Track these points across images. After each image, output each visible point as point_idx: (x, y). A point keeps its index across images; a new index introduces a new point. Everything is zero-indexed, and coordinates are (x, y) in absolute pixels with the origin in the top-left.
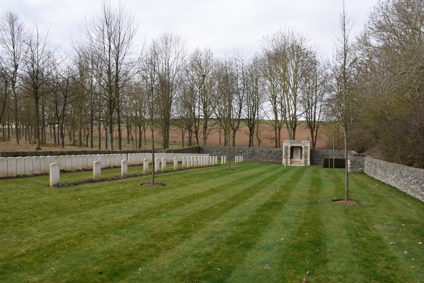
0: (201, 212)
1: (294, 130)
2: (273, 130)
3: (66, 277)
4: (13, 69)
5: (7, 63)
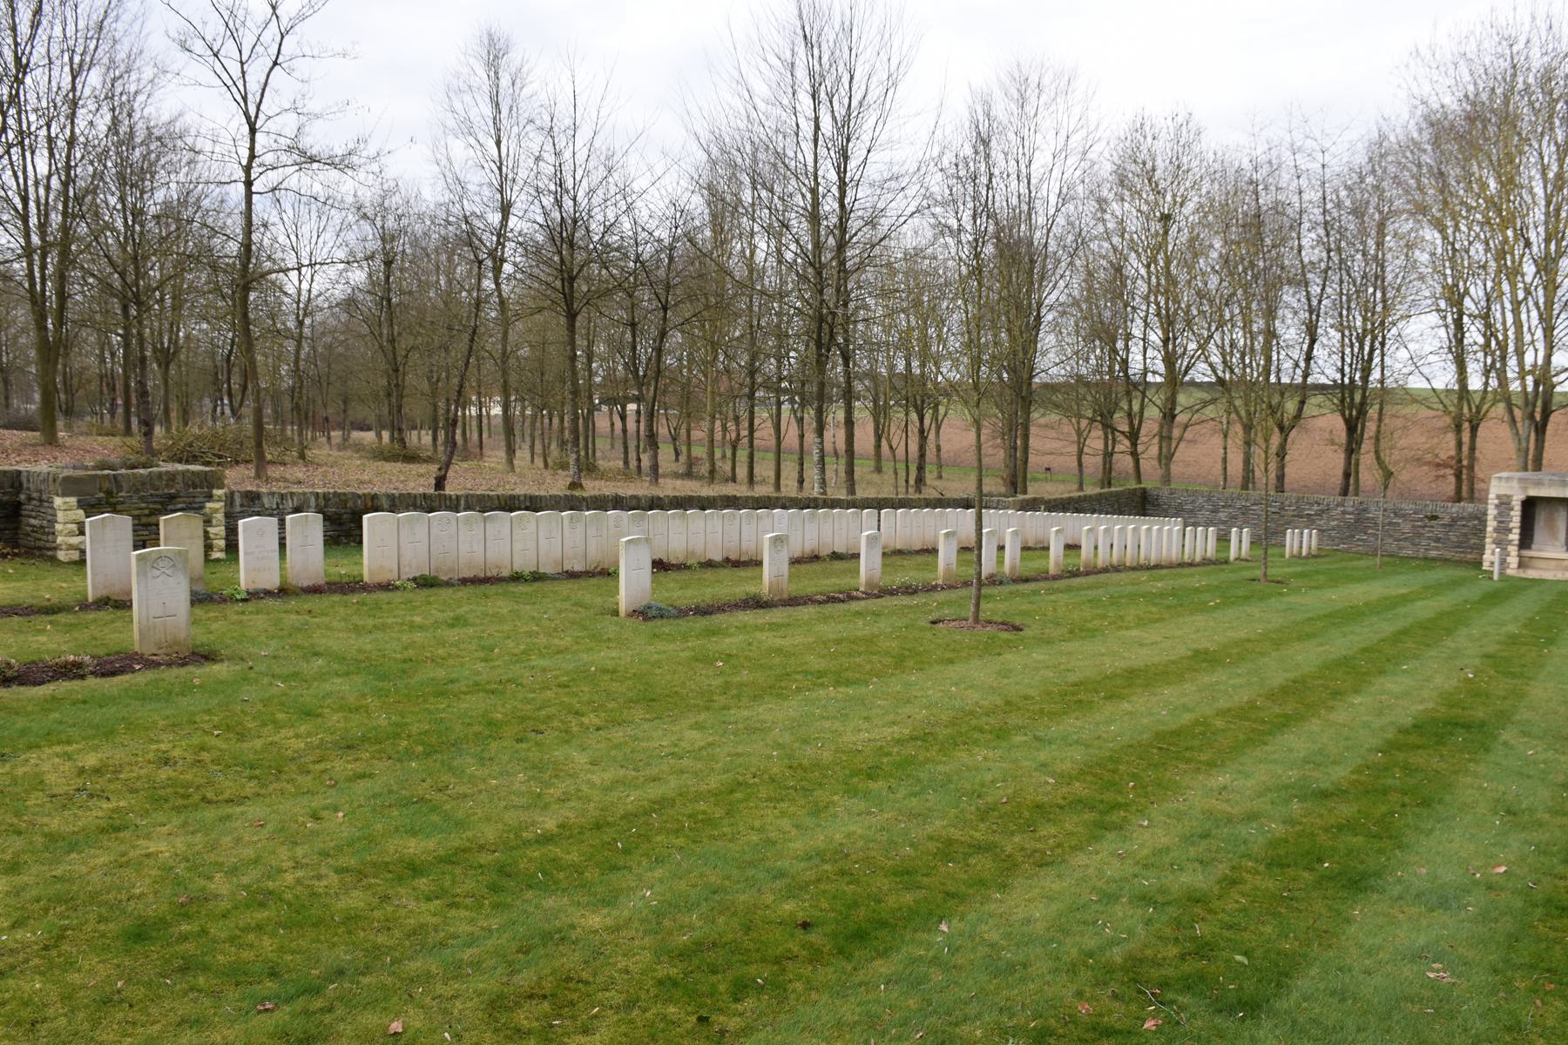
0: (1160, 736)
1: (1541, 429)
2: (1445, 430)
3: (692, 928)
4: (495, 218)
5: (477, 199)
